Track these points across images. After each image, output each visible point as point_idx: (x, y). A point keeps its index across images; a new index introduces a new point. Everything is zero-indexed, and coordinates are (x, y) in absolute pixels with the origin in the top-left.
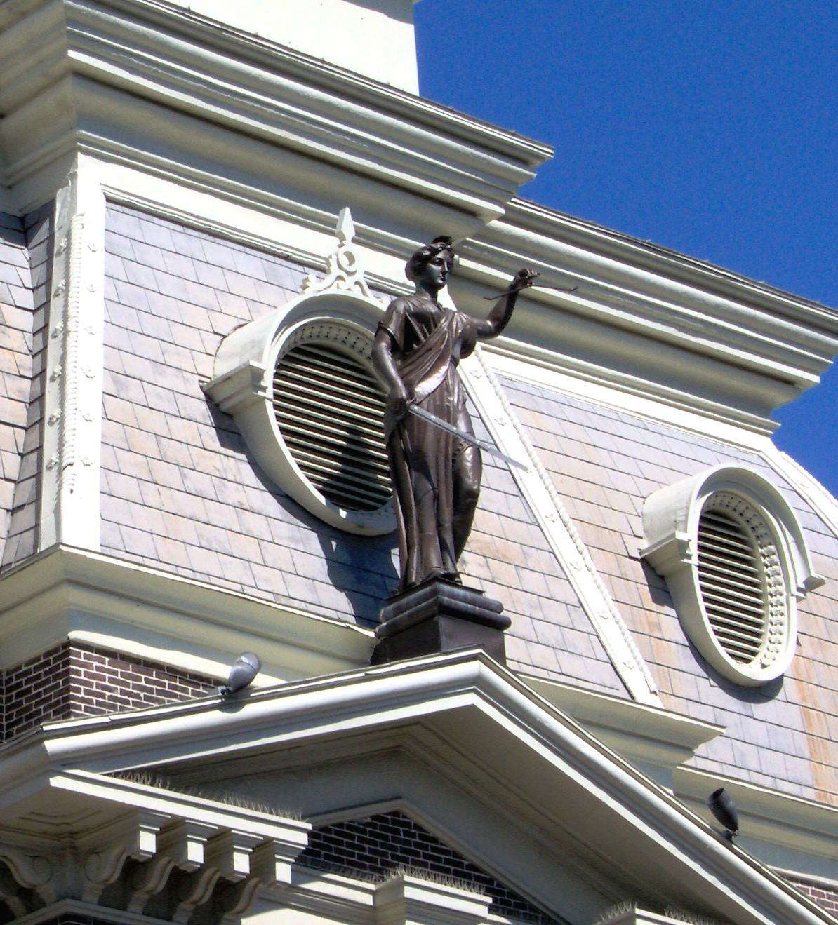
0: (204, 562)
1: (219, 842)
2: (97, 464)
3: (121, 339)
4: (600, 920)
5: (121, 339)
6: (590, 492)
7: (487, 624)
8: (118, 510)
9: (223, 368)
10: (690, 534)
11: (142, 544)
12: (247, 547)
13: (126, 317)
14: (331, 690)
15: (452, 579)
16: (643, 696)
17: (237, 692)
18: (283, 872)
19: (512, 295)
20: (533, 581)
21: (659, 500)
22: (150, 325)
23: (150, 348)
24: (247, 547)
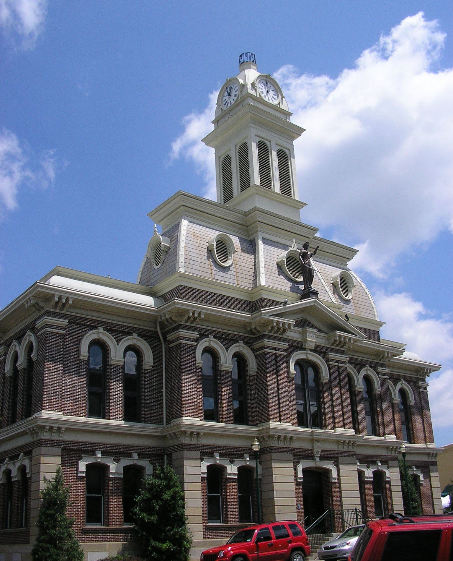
0: (278, 286)
1: (284, 324)
2: (183, 262)
3: (266, 257)
4: (139, 494)
5: (266, 257)
6: (325, 275)
7: (316, 294)
8: (267, 280)
9: (279, 260)
10: (215, 243)
11: (271, 284)
12: (284, 284)
13: (266, 254)
14: (296, 304)
15: (311, 288)
16: (335, 302)
17: (286, 303)
18: (292, 327)
19: (316, 249)
20: (320, 287)
21: (334, 275)
22: (269, 254)
23: (269, 258)
24: (284, 284)
